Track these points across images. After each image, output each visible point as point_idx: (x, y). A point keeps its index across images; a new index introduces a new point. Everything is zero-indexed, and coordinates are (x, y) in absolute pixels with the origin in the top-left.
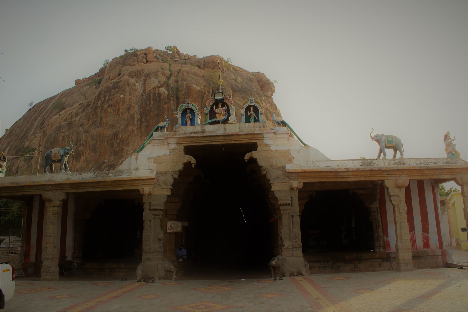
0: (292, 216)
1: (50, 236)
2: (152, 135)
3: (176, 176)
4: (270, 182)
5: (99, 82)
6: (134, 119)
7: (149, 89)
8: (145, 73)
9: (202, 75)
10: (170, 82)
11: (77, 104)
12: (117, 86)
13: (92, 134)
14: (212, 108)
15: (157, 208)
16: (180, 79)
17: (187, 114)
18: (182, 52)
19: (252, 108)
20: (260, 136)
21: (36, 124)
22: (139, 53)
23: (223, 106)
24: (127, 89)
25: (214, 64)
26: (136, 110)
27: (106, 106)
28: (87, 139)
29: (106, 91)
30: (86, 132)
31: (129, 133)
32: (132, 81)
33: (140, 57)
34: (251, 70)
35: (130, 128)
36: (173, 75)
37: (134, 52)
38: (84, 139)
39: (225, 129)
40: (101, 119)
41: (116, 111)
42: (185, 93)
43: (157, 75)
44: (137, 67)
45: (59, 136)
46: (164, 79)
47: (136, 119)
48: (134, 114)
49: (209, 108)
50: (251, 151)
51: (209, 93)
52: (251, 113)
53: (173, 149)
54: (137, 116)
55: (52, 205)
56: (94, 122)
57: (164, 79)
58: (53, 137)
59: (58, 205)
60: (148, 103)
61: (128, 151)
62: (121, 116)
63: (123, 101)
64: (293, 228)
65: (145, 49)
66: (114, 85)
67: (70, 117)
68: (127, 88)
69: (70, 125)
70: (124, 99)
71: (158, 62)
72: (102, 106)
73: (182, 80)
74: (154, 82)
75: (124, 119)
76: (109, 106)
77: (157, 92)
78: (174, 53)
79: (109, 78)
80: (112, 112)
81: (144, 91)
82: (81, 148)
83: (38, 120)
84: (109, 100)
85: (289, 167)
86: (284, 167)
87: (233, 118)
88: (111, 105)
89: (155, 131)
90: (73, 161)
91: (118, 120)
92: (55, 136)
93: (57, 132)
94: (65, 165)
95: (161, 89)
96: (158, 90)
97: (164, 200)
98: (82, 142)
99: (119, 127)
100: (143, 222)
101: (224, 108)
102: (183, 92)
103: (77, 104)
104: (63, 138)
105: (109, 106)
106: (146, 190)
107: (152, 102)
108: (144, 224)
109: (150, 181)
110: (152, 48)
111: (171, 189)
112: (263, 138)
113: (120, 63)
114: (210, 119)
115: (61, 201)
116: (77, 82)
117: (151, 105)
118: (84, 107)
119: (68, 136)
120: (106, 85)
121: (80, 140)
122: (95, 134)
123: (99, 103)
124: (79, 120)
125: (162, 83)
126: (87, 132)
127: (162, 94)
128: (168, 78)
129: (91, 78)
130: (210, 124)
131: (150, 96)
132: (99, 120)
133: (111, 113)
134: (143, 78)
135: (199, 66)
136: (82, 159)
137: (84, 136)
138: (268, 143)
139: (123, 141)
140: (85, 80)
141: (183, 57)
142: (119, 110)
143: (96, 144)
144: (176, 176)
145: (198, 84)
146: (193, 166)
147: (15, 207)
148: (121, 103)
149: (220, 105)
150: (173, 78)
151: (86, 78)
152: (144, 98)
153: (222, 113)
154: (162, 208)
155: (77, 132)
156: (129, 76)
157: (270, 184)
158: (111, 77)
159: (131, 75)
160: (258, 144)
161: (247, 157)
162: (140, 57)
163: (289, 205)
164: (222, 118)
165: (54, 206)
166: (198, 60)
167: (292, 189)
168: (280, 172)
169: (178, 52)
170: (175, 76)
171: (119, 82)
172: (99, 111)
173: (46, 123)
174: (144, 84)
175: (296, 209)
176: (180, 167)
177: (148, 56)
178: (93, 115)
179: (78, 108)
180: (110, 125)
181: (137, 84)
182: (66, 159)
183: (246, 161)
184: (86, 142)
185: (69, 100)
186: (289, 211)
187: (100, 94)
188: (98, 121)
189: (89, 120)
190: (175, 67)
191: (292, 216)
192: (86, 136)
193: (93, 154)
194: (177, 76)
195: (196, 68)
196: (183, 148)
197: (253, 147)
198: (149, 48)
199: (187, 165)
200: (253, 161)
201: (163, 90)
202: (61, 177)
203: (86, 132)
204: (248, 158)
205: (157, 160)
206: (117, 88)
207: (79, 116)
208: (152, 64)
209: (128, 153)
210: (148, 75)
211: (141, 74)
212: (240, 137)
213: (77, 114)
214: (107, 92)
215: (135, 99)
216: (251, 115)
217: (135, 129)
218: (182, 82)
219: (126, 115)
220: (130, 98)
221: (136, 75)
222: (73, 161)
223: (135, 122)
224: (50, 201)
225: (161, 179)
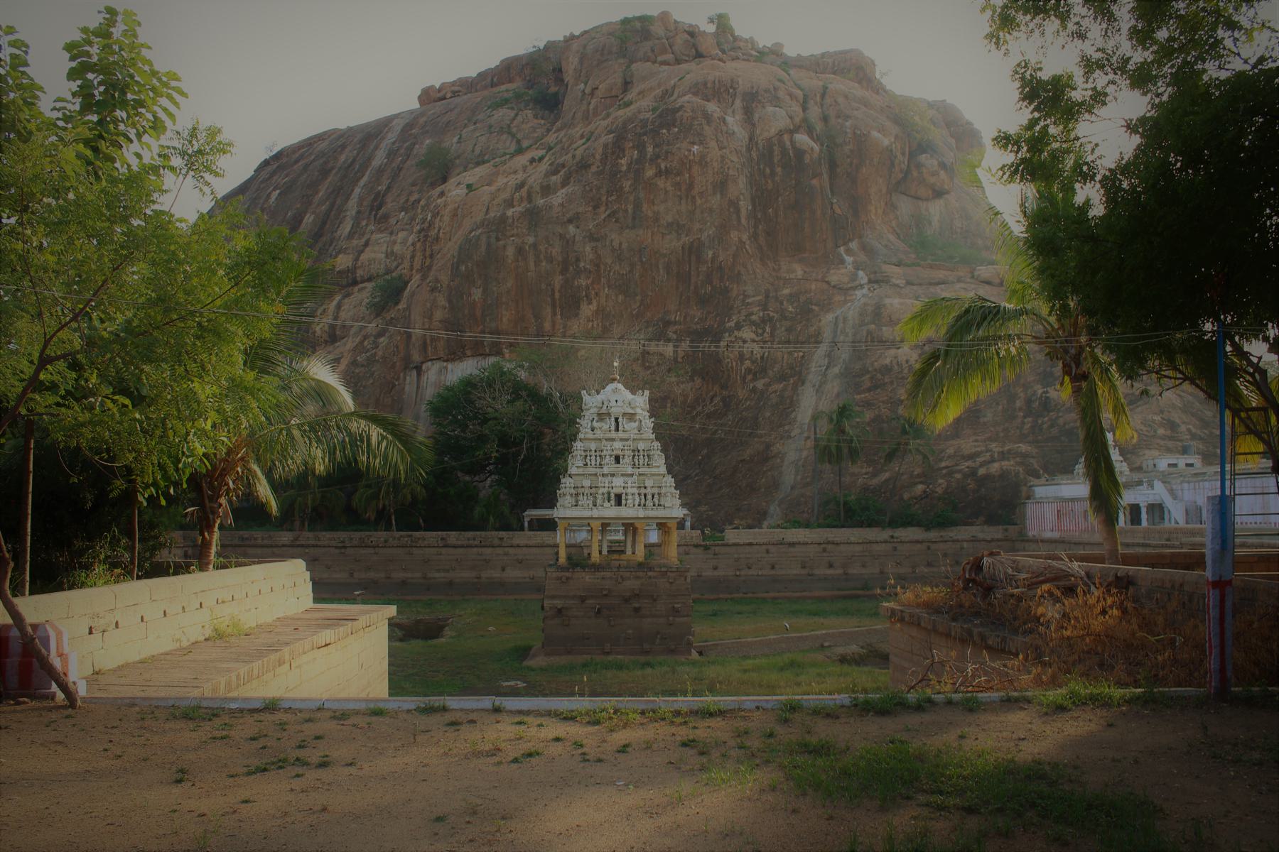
6: (738, 211)
7: (766, 135)
13: (616, 244)
21: (352, 206)
24: (708, 130)
26: (740, 188)
27: (650, 173)
34: (898, 93)
35: (734, 235)
40: (637, 206)
41: (684, 187)
42: (852, 151)
45: (505, 246)
47: (743, 213)
48: (738, 200)
51: (903, 154)
54: (745, 206)
56: (614, 213)
58: (483, 248)
60: (768, 171)
61: (746, 296)
62: (699, 201)
63: (703, 161)
68: (706, 128)
69: (533, 217)
73: (838, 117)
74: (776, 119)
76: (659, 173)
77: (788, 143)
80: (669, 188)
81: (751, 139)
82: (583, 282)
90: (554, 314)
92: (489, 245)
93: (493, 235)
96: (791, 141)
98: (582, 264)
102: (847, 148)
104: (520, 251)
105: (659, 173)
107: (779, 170)
117: (777, 178)
119: (535, 246)
121: (578, 260)
122: (624, 246)
124: (562, 205)
126: (597, 240)
127: (805, 152)
132: (630, 208)
133: (666, 192)
136: (587, 310)
137: (588, 249)
142: (691, 186)
145: (881, 130)
148: (696, 169)
155: (561, 236)
172: (627, 185)
178: (609, 193)
180: (670, 225)
181: (729, 119)
184: (598, 266)
188: (626, 211)
189: (596, 207)
192: (595, 249)
193: (621, 298)
201: (802, 139)
203: (592, 238)
209: (750, 300)
213: (547, 190)
215: (735, 159)
217: (745, 237)
220: (722, 157)
222: (554, 314)
223: (743, 221)
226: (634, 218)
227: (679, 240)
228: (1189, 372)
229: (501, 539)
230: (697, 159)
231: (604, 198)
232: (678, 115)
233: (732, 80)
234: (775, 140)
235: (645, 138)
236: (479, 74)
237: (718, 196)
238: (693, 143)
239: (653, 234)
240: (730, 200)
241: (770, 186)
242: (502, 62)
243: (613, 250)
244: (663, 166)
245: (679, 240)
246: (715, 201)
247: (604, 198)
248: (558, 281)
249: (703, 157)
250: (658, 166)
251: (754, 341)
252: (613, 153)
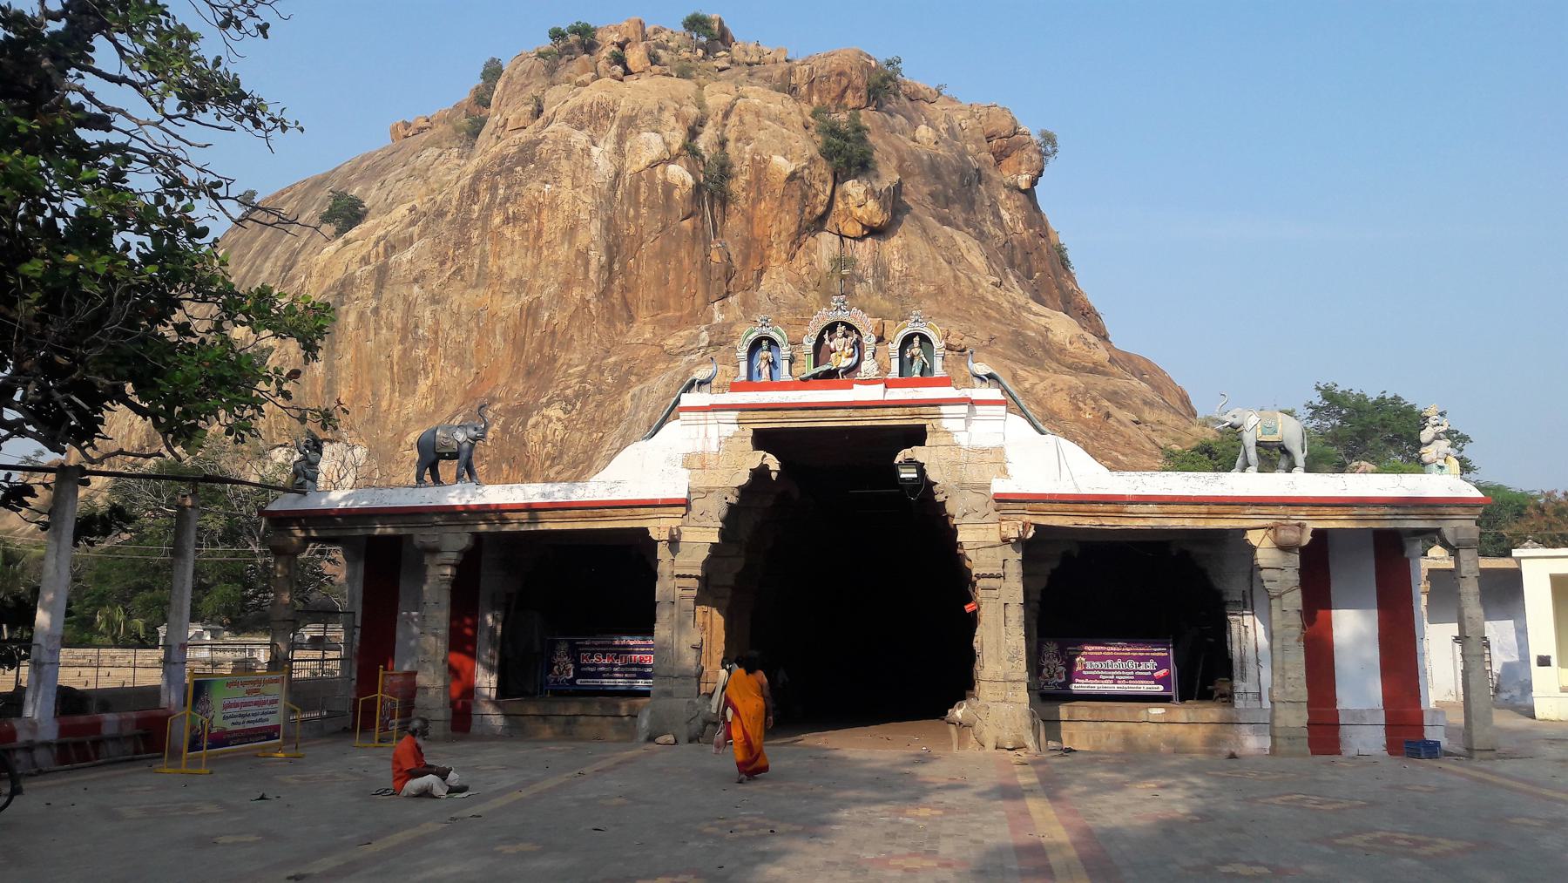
3: (734, 500)
5: (474, 133)
6: (587, 263)
7: (635, 168)
11: (402, 210)
12: (534, 155)
14: (820, 340)
16: (731, 135)
19: (917, 339)
24: (565, 166)
25: (844, 82)
27: (497, 220)
28: (437, 323)
32: (580, 138)
35: (577, 292)
40: (483, 260)
42: (748, 182)
43: (659, 121)
47: (594, 265)
49: (814, 339)
54: (597, 257)
56: (460, 269)
57: (678, 138)
60: (632, 212)
61: (570, 366)
63: (554, 206)
66: (521, 151)
67: (381, 249)
68: (563, 162)
69: (382, 276)
72: (486, 217)
73: (738, 140)
75: (556, 264)
76: (506, 221)
81: (617, 175)
82: (421, 352)
83: (274, 255)
84: (507, 199)
87: (868, 367)
88: (515, 218)
90: (393, 391)
91: (536, 267)
95: (672, 168)
97: (704, 554)
98: (420, 331)
100: (654, 605)
102: (742, 179)
103: (402, 210)
106: (658, 528)
121: (417, 327)
122: (463, 308)
123: (476, 208)
124: (411, 261)
127: (676, 186)
128: (693, 133)
131: (638, 189)
134: (614, 130)
136: (424, 385)
137: (427, 313)
139: (553, 333)
142: (539, 234)
143: (467, 339)
144: (734, 500)
146: (774, 475)
147: (336, 568)
148: (545, 213)
155: (405, 299)
158: (511, 120)
159: (577, 120)
160: (928, 428)
163: (998, 577)
164: (846, 362)
171: (537, 143)
173: (300, 265)
174: (620, 151)
175: (1013, 589)
176: (743, 478)
178: (457, 245)
179: (407, 220)
180: (513, 282)
181: (595, 151)
184: (436, 333)
185: (374, 192)
187: (477, 177)
189: (442, 263)
192: (434, 312)
193: (457, 370)
199: (760, 474)
203: (434, 300)
206: (532, 162)
215: (588, 199)
217: (590, 295)
219: (563, 252)
220: (574, 198)
223: (592, 276)
227: (518, 298)
229: (114, 658)
243: (453, 314)
245: (518, 298)
246: (563, 252)
248: (397, 351)
251: (559, 419)
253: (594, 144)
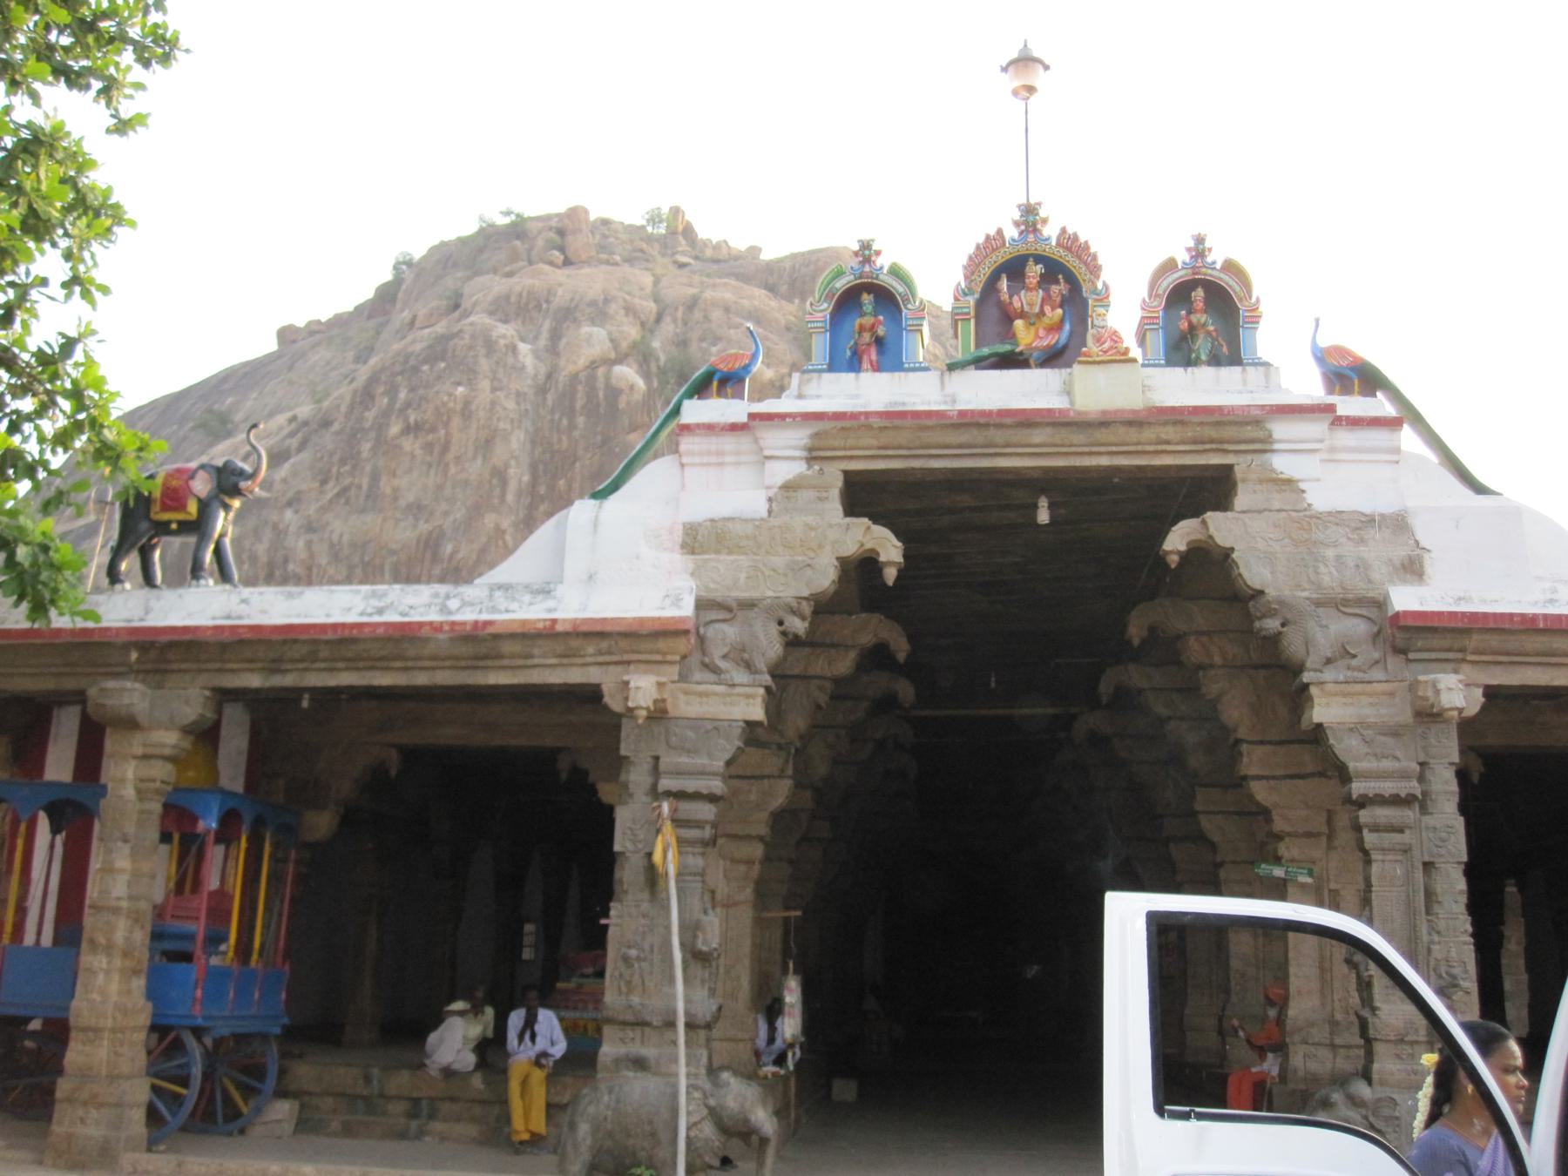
0: (1428, 866)
1: (116, 911)
2: (676, 411)
4: (1306, 677)
6: (504, 483)
7: (571, 368)
8: (554, 306)
9: (783, 322)
10: (656, 344)
11: (281, 419)
13: (335, 538)
15: (691, 785)
17: (862, 315)
18: (703, 233)
19: (1199, 294)
20: (1250, 432)
22: (533, 227)
23: (1048, 279)
24: (484, 364)
26: (515, 446)
27: (395, 429)
28: (312, 556)
29: (398, 368)
30: (309, 528)
31: (484, 539)
32: (505, 331)
33: (540, 242)
35: (490, 520)
36: (667, 319)
37: (513, 224)
38: (304, 555)
39: (1068, 392)
40: (375, 478)
41: (437, 450)
44: (525, 282)
46: (633, 332)
47: (512, 486)
50: (1196, 512)
52: (1194, 318)
53: (788, 487)
54: (518, 475)
55: (140, 751)
56: (345, 490)
59: (167, 751)
60: (565, 422)
62: (453, 470)
63: (466, 412)
64: (1433, 929)
65: (558, 215)
66: (430, 347)
70: (467, 403)
71: (608, 263)
72: (381, 427)
74: (593, 340)
75: (466, 483)
76: (408, 430)
78: (672, 232)
79: (412, 323)
81: (549, 376)
84: (408, 405)
85: (1405, 599)
86: (1380, 604)
89: (690, 394)
91: (440, 487)
94: (218, 552)
95: (618, 369)
98: (291, 567)
99: (446, 514)
101: (1055, 289)
103: (281, 419)
105: (408, 430)
108: (617, 875)
109: (662, 644)
110: (586, 212)
111: (768, 689)
112: (1264, 445)
113: (455, 265)
114: (978, 346)
115: (187, 730)
116: (287, 335)
117: (576, 434)
118: (306, 431)
120: (397, 346)
121: (286, 561)
122: (346, 539)
124: (284, 481)
125: (624, 345)
129: (340, 321)
130: (980, 363)
132: (365, 482)
133: (413, 457)
134: (547, 325)
135: (772, 289)
137: (301, 544)
138: (1296, 475)
140: (316, 328)
141: (709, 253)
142: (445, 448)
146: (890, 575)
148: (456, 422)
149: (1034, 271)
150: (668, 328)
151: (319, 322)
152: (550, 402)
153: (1042, 313)
154: (717, 786)
156: (491, 313)
157: (1306, 686)
159: (503, 309)
160: (1239, 472)
161: (1177, 540)
162: (540, 242)
165: (146, 757)
166: (770, 267)
167: (1428, 715)
168: (1360, 628)
169: (688, 232)
170: (675, 320)
172: (366, 447)
174: (553, 350)
176: (825, 577)
177: (570, 238)
178: (343, 462)
179: (286, 432)
180: (409, 507)
181: (524, 348)
182: (221, 522)
183: (1173, 560)
184: (310, 569)
186: (1406, 837)
187: (373, 380)
188: (360, 487)
189: (324, 482)
190: (678, 288)
191: (1428, 866)
192: (309, 544)
194: (685, 323)
195: (760, 293)
196: (839, 482)
197: (1211, 489)
198: (575, 213)
200: (1211, 563)
201: (627, 374)
202: (200, 606)
203: (309, 528)
204: (1183, 548)
205: (699, 540)
206: (443, 359)
207: (287, 466)
208: (586, 270)
210: (567, 315)
211: (539, 307)
212: (1148, 434)
214: (401, 373)
215: (511, 404)
216: (1192, 328)
218: (704, 345)
220: (493, 403)
221: (520, 309)
223: (510, 498)
224: (131, 724)
225: (725, 634)
226: (368, 497)
228: (821, 769)
230: (458, 407)
231: (334, 470)
232: (452, 343)
233: (549, 291)
234: (582, 376)
235: (399, 378)
236: (357, 308)
237: (479, 461)
238: (459, 384)
239: (385, 520)
240: (494, 468)
241: (565, 444)
242: (378, 290)
243: (332, 546)
244: (412, 419)
247: (334, 470)
249: (467, 403)
250: (406, 420)
252: (361, 403)
253: (523, 340)
